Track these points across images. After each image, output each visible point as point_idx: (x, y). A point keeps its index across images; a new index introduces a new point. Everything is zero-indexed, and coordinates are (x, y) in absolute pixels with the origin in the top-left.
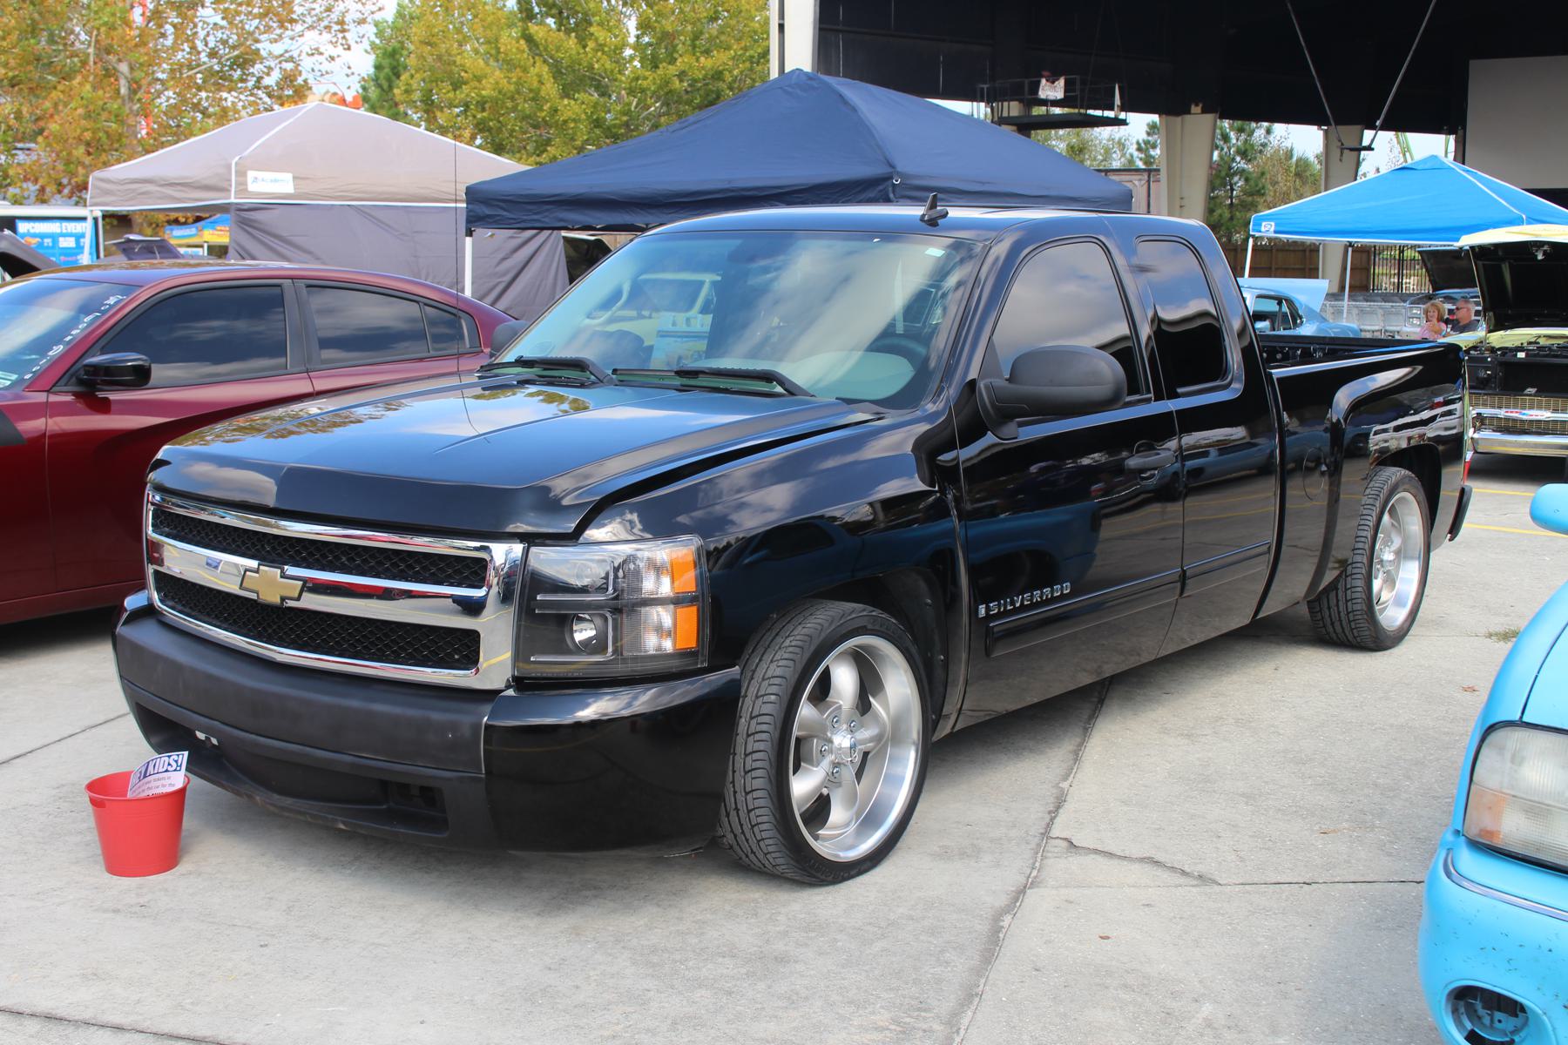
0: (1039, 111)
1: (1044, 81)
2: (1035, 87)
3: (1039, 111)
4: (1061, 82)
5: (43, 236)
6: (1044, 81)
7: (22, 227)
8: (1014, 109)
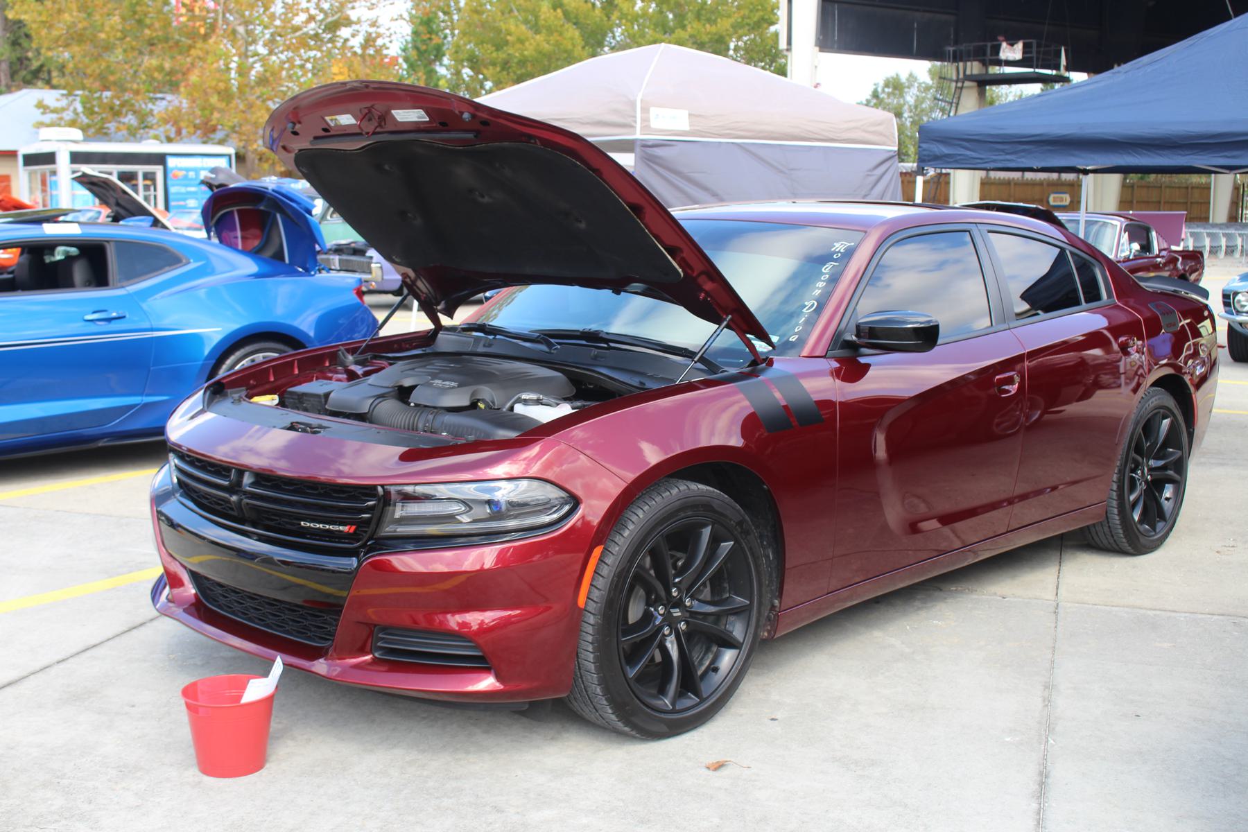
0: (995, 70)
1: (1004, 45)
2: (997, 49)
3: (995, 70)
4: (1020, 46)
5: (188, 170)
6: (1004, 45)
7: (171, 162)
8: (974, 68)
